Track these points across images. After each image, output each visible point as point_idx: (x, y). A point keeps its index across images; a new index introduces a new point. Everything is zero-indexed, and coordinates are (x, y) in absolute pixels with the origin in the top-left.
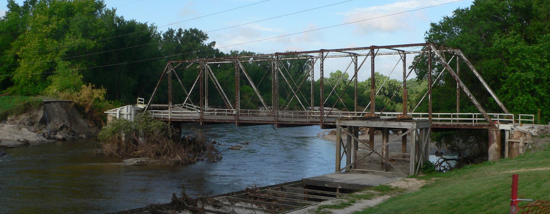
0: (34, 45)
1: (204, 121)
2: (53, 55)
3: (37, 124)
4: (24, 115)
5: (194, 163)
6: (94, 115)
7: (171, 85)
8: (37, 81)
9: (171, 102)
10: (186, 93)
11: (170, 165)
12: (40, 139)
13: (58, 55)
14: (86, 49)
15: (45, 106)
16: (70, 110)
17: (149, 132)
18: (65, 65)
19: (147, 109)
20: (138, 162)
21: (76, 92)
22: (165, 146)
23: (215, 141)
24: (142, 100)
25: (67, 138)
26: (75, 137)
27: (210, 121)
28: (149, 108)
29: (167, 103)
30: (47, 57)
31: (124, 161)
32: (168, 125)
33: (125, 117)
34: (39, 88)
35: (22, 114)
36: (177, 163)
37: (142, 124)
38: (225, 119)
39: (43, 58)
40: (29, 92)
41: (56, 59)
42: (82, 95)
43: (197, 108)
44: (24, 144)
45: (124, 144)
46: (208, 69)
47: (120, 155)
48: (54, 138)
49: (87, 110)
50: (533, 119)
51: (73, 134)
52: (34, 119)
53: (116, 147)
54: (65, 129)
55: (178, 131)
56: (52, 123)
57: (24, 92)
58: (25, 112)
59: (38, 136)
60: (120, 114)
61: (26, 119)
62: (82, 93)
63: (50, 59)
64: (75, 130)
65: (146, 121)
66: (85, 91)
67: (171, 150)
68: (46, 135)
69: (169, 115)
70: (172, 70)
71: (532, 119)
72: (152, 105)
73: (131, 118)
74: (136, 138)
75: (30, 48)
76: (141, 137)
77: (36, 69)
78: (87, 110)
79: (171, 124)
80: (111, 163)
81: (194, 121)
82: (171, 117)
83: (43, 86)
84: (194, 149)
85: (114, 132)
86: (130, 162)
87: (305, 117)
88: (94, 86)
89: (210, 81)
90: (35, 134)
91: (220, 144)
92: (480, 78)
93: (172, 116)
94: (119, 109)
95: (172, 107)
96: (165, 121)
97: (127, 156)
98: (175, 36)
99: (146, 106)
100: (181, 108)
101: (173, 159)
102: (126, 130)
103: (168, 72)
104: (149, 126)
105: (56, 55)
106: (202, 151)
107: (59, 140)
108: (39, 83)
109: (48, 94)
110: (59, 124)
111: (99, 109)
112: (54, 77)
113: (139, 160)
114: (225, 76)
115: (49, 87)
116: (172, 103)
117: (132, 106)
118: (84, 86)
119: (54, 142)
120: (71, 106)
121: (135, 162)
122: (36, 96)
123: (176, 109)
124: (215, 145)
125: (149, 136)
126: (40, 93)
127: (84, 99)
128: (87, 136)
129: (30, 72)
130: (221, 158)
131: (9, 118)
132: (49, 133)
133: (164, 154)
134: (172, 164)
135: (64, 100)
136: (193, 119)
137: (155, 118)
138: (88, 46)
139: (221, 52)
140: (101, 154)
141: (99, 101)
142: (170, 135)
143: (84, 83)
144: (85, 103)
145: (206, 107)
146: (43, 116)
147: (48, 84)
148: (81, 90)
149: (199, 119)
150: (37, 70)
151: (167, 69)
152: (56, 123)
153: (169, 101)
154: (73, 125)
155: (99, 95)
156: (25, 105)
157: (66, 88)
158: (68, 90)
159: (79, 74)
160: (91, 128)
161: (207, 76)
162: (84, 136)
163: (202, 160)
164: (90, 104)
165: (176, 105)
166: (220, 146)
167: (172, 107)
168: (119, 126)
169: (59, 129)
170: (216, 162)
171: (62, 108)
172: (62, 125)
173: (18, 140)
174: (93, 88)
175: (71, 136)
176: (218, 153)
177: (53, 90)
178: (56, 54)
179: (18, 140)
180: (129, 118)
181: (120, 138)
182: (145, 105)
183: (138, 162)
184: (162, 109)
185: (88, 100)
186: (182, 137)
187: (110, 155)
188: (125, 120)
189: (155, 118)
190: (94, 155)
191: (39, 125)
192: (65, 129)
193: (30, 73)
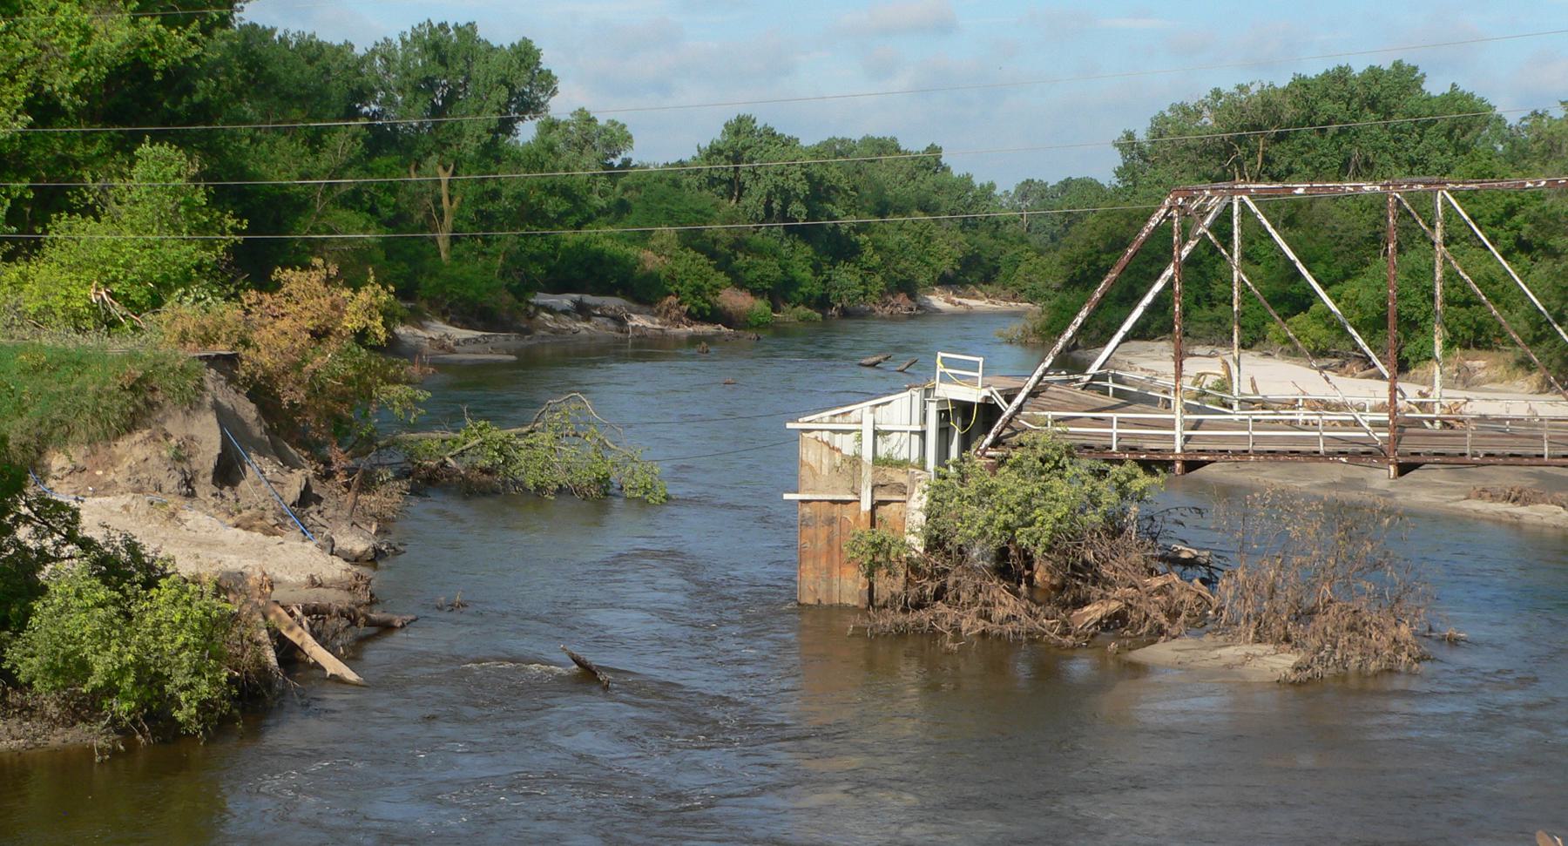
24: (973, 367)
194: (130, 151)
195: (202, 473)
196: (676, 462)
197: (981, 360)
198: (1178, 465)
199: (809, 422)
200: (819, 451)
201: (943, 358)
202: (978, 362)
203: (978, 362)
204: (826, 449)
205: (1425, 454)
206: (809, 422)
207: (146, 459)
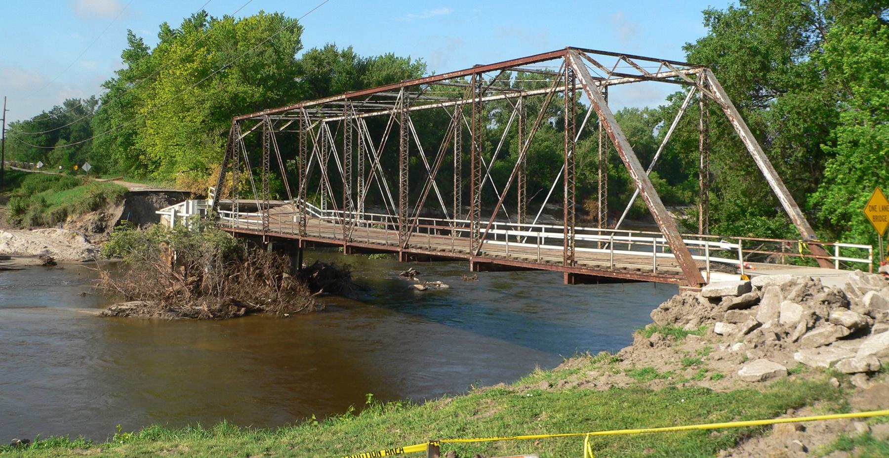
50: (870, 258)
58: (93, 210)
60: (177, 218)
71: (867, 258)
87: (353, 99)
92: (747, 140)
98: (312, 276)
131: (69, 219)
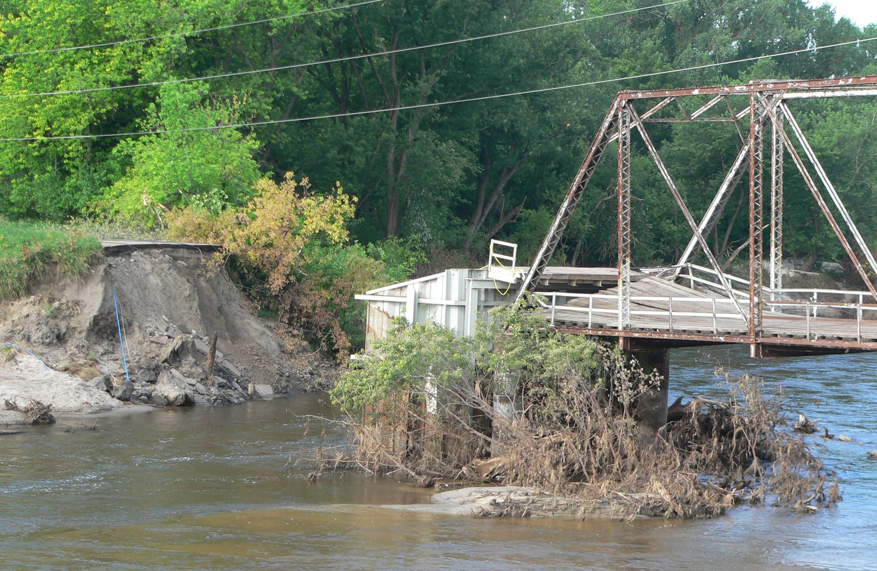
0: (54, 10)
1: (766, 340)
2: (132, 49)
3: (78, 339)
4: (24, 300)
5: (723, 512)
6: (305, 303)
7: (628, 189)
8: (69, 159)
9: (628, 260)
10: (692, 223)
11: (622, 520)
12: (92, 403)
13: (152, 50)
14: (270, 28)
15: (110, 266)
16: (209, 281)
17: (540, 384)
18: (189, 97)
19: (529, 287)
20: (495, 504)
21: (230, 209)
22: (603, 441)
23: (812, 421)
24: (508, 251)
25: (198, 398)
26: (231, 392)
27: (792, 342)
28: (537, 285)
29: (611, 261)
30: (107, 60)
31: (436, 497)
32: (617, 353)
33: (438, 317)
34: (77, 189)
35: (18, 297)
36: (656, 512)
37: (508, 351)
38: (852, 335)
39: (92, 64)
40: (33, 204)
41: (148, 69)
42: (258, 222)
43: (735, 285)
44: (32, 419)
45: (432, 428)
46: (786, 123)
47: (419, 474)
48: (149, 399)
49: (277, 282)
51: (222, 380)
52: (64, 318)
53: (399, 439)
54: (191, 359)
55: (657, 379)
56: (138, 335)
57: (12, 204)
58: (29, 292)
59: (86, 387)
61: (33, 318)
62: (257, 213)
63: (119, 70)
64: (229, 366)
65: (526, 334)
66: (270, 205)
67: (625, 457)
68: (115, 384)
69: (619, 312)
70: (632, 126)
72: (550, 271)
73: (462, 321)
74: (484, 405)
75: (39, 20)
76: (504, 400)
77: (62, 108)
78: (277, 282)
79: (624, 352)
80: (383, 506)
81: (722, 339)
82: (628, 322)
83: (92, 180)
84: (722, 458)
85: (398, 381)
86: (463, 503)
88: (305, 182)
89: (790, 174)
90: (74, 382)
91: (831, 437)
93: (633, 317)
94: (414, 285)
95: (634, 280)
96: (604, 338)
97: (446, 478)
99: (526, 273)
100: (669, 285)
101: (637, 496)
102: (445, 374)
103: (614, 137)
104: (538, 357)
105: (145, 52)
106: (755, 464)
107: (169, 404)
108: (74, 167)
109: (117, 212)
110: (165, 339)
111: (324, 279)
112: (140, 146)
113: (501, 494)
114: (858, 131)
115: (118, 184)
116: (631, 265)
117: (466, 271)
118: (264, 183)
119: (149, 413)
120: (210, 264)
121: (485, 503)
122: (64, 220)
123: (648, 287)
124: (809, 439)
125: (540, 399)
126: (83, 210)
127: (264, 239)
128: (276, 390)
129: (40, 122)
130: (837, 498)
132: (128, 377)
133: (599, 470)
134: (631, 517)
135: (184, 241)
136: (720, 334)
137: (563, 323)
138: (277, 14)
139: (842, 20)
140: (342, 467)
141: (322, 246)
142: (626, 398)
143: (264, 170)
144: (268, 253)
145: (774, 289)
146: (102, 305)
147: (111, 171)
148: (251, 199)
149: (744, 334)
150: (66, 111)
151: (611, 125)
152: (152, 334)
153: (621, 256)
154: (220, 343)
155: (327, 222)
156: (31, 261)
157: (192, 192)
158: (201, 199)
159: (245, 131)
160: (291, 354)
161: (781, 153)
162: (265, 390)
163: (755, 501)
164: (290, 257)
165: (646, 271)
166: (830, 444)
167: (634, 280)
168: (419, 354)
169: (165, 361)
170: (814, 512)
171: (175, 273)
172: (176, 343)
173: (7, 403)
174: (300, 191)
175: (214, 390)
176: (823, 474)
177: (138, 200)
178: (147, 45)
179: (7, 403)
180: (454, 324)
181: (416, 402)
182: (522, 270)
183: (495, 504)
184: (589, 287)
185: (281, 243)
186: (672, 399)
187: (381, 471)
188: (441, 331)
189: (560, 323)
190: (316, 468)
191: (85, 342)
192: (191, 359)
193: (38, 124)
194: (121, 108)
195: (79, 330)
196: (838, 388)
197: (515, 246)
198: (621, 341)
199: (373, 294)
200: (381, 319)
201: (495, 245)
202: (513, 248)
203: (513, 248)
204: (385, 318)
205: (781, 336)
206: (373, 294)
207: (28, 316)
